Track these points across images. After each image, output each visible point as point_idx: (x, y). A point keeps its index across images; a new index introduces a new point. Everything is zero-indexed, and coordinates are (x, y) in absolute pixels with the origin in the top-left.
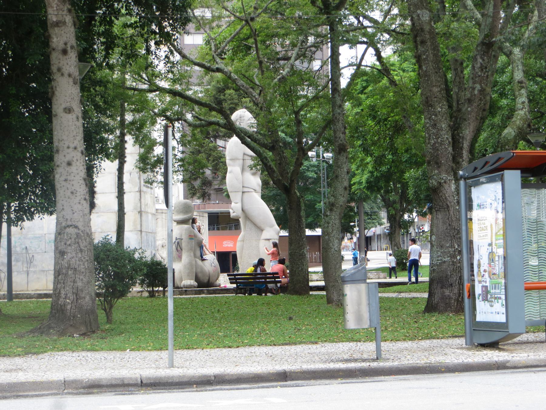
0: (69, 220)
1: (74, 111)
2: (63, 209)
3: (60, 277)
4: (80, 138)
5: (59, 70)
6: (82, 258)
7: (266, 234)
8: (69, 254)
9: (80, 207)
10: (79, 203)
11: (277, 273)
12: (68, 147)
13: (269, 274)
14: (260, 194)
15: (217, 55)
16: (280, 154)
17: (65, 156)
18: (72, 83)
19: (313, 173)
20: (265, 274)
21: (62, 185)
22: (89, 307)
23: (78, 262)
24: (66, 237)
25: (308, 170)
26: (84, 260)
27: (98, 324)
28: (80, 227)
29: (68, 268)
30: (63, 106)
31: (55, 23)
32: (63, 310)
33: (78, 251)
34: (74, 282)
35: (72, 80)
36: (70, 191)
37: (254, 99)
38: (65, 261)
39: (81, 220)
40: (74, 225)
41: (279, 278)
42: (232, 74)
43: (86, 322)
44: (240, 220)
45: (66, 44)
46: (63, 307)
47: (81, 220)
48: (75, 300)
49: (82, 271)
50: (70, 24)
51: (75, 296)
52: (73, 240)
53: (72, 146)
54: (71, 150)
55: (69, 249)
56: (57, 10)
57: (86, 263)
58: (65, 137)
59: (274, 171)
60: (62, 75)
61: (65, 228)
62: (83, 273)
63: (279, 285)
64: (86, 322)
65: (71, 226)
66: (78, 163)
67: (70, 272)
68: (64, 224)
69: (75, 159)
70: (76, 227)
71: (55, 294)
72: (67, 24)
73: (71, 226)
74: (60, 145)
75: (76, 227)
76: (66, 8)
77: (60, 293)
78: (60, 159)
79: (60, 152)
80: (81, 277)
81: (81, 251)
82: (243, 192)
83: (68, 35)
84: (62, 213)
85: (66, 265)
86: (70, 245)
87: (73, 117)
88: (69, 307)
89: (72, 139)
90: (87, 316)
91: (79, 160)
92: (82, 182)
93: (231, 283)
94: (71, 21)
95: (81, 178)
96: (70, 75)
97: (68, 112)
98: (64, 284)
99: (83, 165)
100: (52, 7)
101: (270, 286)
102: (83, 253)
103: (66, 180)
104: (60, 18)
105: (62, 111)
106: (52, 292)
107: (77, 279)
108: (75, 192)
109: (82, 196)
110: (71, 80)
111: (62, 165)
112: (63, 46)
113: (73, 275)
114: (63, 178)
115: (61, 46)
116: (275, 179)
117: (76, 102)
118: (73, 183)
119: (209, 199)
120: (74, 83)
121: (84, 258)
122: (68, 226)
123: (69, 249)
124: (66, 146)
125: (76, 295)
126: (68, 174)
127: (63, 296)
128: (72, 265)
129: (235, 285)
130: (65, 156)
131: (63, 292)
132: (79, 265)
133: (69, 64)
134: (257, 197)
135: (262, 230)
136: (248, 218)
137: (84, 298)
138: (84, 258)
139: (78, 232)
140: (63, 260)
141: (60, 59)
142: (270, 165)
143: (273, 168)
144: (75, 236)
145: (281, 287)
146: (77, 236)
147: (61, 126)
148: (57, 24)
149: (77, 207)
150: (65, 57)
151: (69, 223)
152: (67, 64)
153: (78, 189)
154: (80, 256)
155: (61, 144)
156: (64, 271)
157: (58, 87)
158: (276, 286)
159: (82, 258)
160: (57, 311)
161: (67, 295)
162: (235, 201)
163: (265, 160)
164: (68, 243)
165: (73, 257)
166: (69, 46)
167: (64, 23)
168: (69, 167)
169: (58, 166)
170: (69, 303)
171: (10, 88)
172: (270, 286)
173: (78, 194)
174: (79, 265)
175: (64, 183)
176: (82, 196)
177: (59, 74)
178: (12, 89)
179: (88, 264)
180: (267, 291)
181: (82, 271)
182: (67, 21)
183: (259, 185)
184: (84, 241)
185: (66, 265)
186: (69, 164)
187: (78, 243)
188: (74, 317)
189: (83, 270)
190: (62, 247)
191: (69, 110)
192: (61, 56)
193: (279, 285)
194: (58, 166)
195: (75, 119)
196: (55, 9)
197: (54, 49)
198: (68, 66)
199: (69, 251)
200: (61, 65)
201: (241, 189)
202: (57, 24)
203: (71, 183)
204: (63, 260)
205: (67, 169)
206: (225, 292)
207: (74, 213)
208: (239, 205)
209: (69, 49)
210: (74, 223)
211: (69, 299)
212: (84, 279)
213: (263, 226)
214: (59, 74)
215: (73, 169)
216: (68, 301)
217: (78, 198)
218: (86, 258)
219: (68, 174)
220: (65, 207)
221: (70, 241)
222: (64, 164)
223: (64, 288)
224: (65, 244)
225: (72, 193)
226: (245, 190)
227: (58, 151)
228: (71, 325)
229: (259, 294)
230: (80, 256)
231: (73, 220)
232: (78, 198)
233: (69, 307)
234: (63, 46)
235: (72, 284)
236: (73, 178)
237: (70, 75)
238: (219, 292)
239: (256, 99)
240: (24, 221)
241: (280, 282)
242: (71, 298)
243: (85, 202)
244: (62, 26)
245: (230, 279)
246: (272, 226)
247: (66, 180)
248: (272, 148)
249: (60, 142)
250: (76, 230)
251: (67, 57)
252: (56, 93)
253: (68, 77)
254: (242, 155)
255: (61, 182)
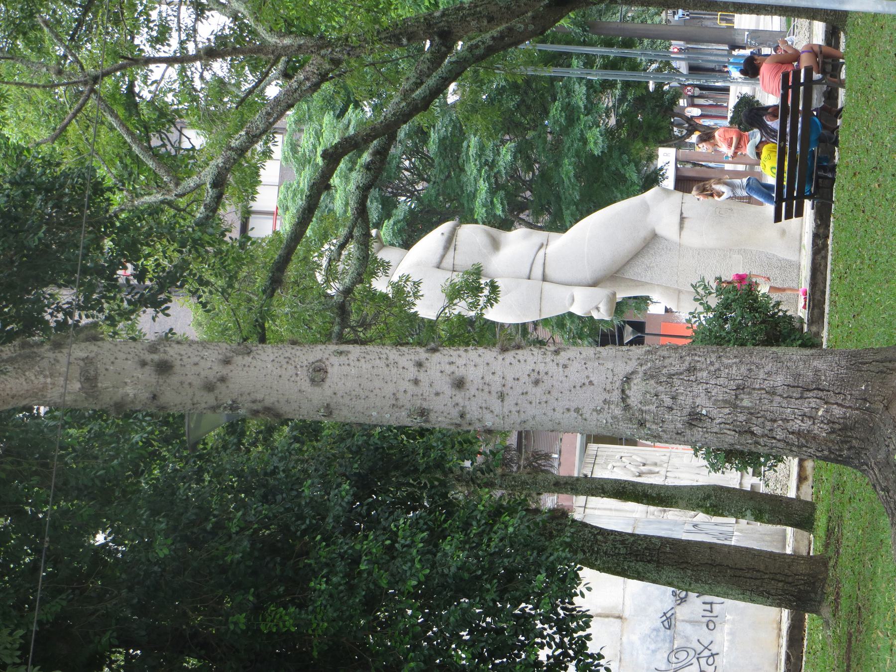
0: (607, 396)
1: (320, 361)
2: (577, 410)
3: (755, 429)
4: (394, 351)
5: (209, 387)
6: (712, 368)
7: (667, 226)
8: (698, 401)
9: (575, 366)
10: (565, 366)
11: (785, 77)
12: (416, 382)
13: (784, 98)
14: (553, 234)
15: (177, 184)
16: (463, 19)
17: (437, 394)
18: (248, 359)
19: (503, 151)
20: (783, 111)
21: (514, 409)
22: (843, 363)
23: (721, 381)
24: (653, 408)
25: (492, 165)
26: (717, 365)
27: (888, 347)
28: (629, 369)
29: (735, 406)
30: (306, 385)
31: (87, 385)
32: (845, 428)
33: (692, 378)
34: (772, 392)
35: (240, 357)
36: (530, 388)
37: (308, 84)
38: (714, 413)
39: (610, 365)
40: (623, 383)
41: (797, 73)
42: (234, 143)
43: (882, 372)
44: (620, 296)
45: (143, 364)
46: (837, 426)
47: (610, 365)
48: (821, 394)
49: (746, 373)
50: (95, 349)
51: (810, 394)
52: (660, 388)
53: (412, 372)
54: (422, 376)
55: (686, 401)
56: (52, 375)
57: (726, 361)
58: (389, 389)
59: (510, 29)
60: (223, 380)
61: (627, 408)
62: (750, 370)
63: (816, 76)
64: (882, 372)
65: (623, 391)
66: (460, 362)
67: (746, 403)
68: (618, 412)
69: (449, 369)
70: (628, 379)
71: (800, 447)
72: (92, 355)
73: (623, 391)
74: (408, 406)
75: (628, 379)
76: (51, 355)
77: (798, 434)
78: (444, 412)
79: (425, 405)
80: (762, 375)
81: (692, 370)
82: (544, 279)
83: (121, 356)
84: (587, 416)
85: (727, 411)
86: (673, 398)
87: (337, 364)
88: (837, 411)
89: (394, 371)
90: (865, 367)
91: (452, 359)
92: (509, 356)
93: (800, 214)
94: (83, 345)
95: (500, 357)
96: (227, 362)
97: (322, 375)
98: (775, 421)
99: (466, 351)
100: (45, 387)
101: (817, 101)
102: (698, 365)
103: (502, 396)
104: (75, 371)
105: (318, 390)
106: (786, 613)
107: (766, 385)
108: (534, 376)
109: (548, 360)
110: (239, 360)
111: (461, 401)
112: (148, 370)
113: (755, 394)
114: (496, 405)
115: (147, 375)
116: (531, 27)
117: (298, 353)
118: (509, 377)
119: (547, 457)
120: (249, 354)
121: (712, 363)
122: (624, 398)
123: (686, 401)
124: (411, 388)
125: (808, 390)
126: (486, 388)
127: (806, 425)
128: (727, 397)
129: (808, 204)
130: (437, 394)
131: (797, 425)
132: (730, 378)
133: (197, 359)
134: (559, 242)
135: (654, 238)
136: (618, 271)
137: (817, 371)
138: (712, 363)
139: (641, 375)
140: (712, 419)
141: (182, 383)
142: (493, 38)
143: (501, 32)
144: (652, 382)
145: (823, 71)
146: (652, 377)
147: (358, 397)
148: (90, 380)
149: (576, 373)
150: (177, 368)
151: (616, 396)
152: (196, 364)
153: (529, 368)
154: (705, 374)
155: (404, 400)
156: (742, 418)
157: (253, 396)
158: (819, 82)
159: (712, 368)
160: (846, 442)
161: (804, 415)
162: (567, 303)
163: (477, 52)
164: (668, 401)
165: (707, 391)
166: (148, 357)
167: (88, 361)
168: (467, 385)
169: (462, 416)
170: (827, 411)
171: (232, 627)
172: (817, 101)
173: (541, 367)
174: (730, 378)
175: (509, 402)
176: (548, 360)
177: (221, 387)
178: (236, 624)
179: (728, 358)
180: (831, 111)
181: (746, 373)
182: (83, 355)
183: (525, 237)
184: (667, 361)
185: (727, 411)
186: (460, 384)
187: (670, 376)
188: (865, 400)
189: (743, 369)
190: (676, 419)
191: (318, 373)
192: (174, 380)
193: (816, 76)
194: (462, 416)
195: (343, 359)
196: (49, 380)
197: (154, 397)
198: (202, 363)
199: (689, 401)
200: (197, 382)
201: (536, 283)
202: (90, 380)
203: (510, 382)
204: (712, 419)
205: (473, 391)
206: (819, 277)
207: (591, 383)
208: (580, 293)
209: (156, 357)
210: (618, 384)
211: (818, 409)
212: (768, 368)
213: (643, 234)
214: (221, 387)
215: (473, 375)
216: (820, 413)
217: (552, 368)
218: (713, 359)
219: (486, 388)
220: (574, 405)
221: (663, 396)
222: (459, 397)
223: (786, 420)
224: (671, 409)
225: (536, 383)
226: (538, 272)
227: (423, 413)
228: (887, 408)
229: (830, 140)
230: (705, 374)
231: (609, 387)
232: (552, 368)
233: (837, 411)
234: (148, 370)
235: (778, 399)
236: (497, 378)
237: (227, 362)
238: (818, 294)
239: (307, 79)
240: (588, 637)
241: (809, 71)
242: (813, 403)
243: (562, 353)
244: (96, 369)
245: (789, 216)
246: (646, 208)
247: (502, 396)
248: (446, 38)
249: (400, 403)
250: (637, 380)
251: (178, 363)
252: (267, 403)
253: (230, 367)
254: (439, 272)
255: (506, 411)
